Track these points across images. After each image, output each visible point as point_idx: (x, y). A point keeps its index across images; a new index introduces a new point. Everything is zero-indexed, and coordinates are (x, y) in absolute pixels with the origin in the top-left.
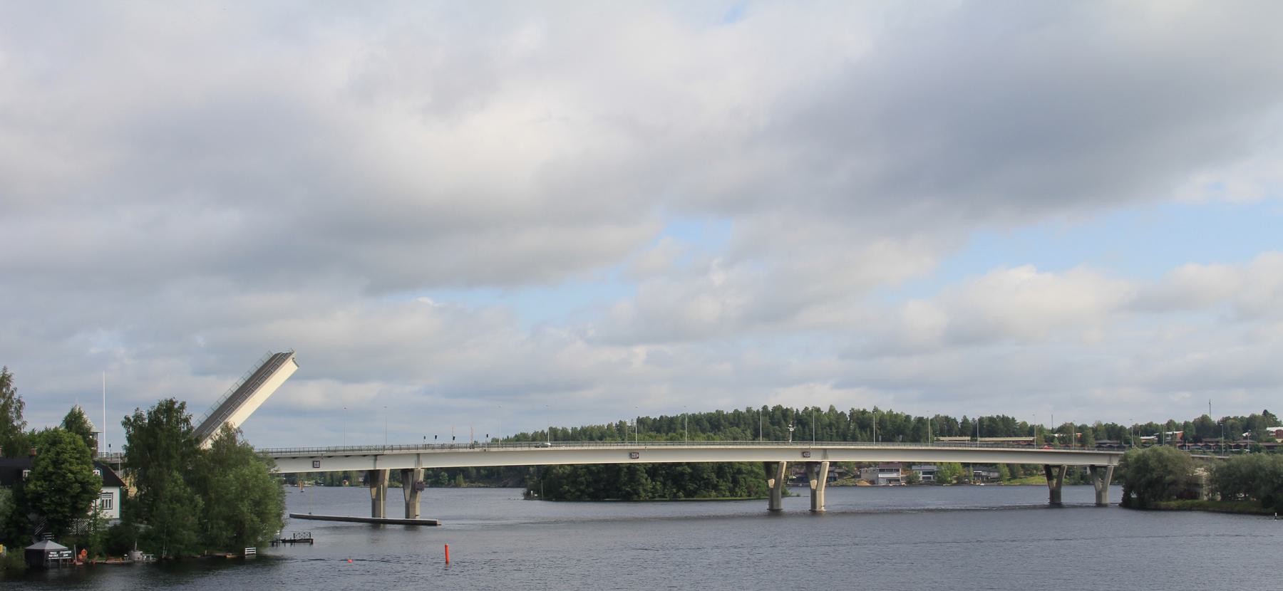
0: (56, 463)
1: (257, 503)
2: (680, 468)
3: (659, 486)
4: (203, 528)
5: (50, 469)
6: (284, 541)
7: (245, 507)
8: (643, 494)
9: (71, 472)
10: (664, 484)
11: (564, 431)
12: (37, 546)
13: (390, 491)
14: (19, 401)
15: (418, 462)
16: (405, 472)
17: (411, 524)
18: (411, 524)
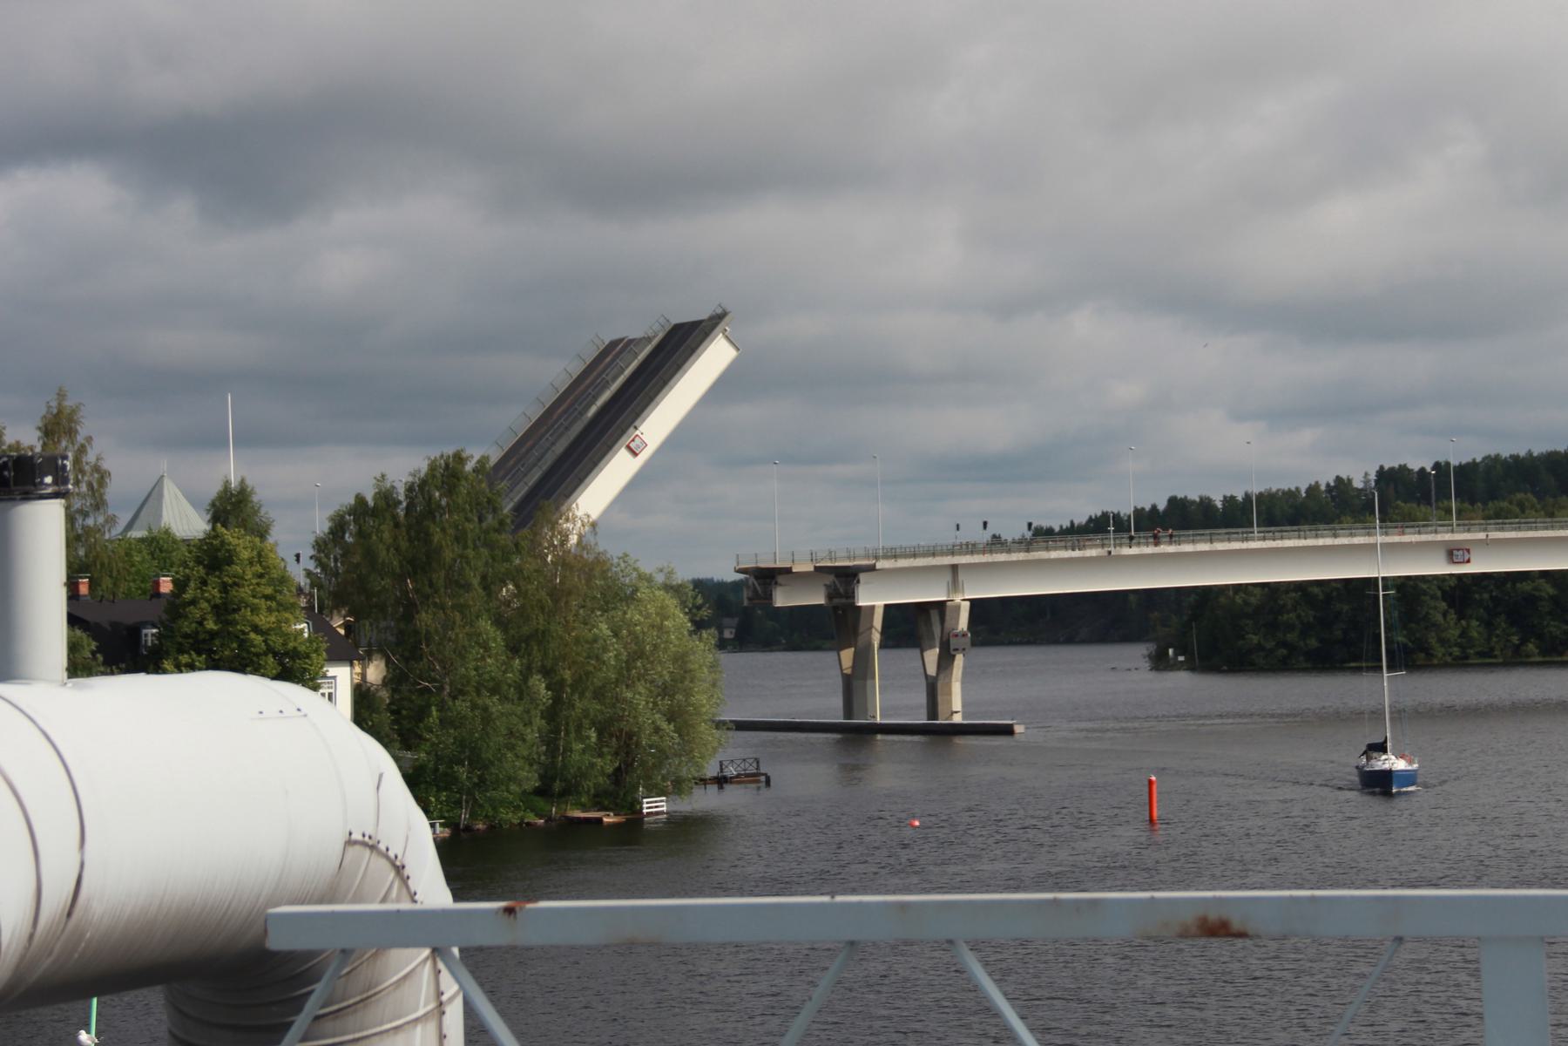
0: (224, 610)
1: (666, 691)
2: (1526, 587)
3: (1475, 630)
5: (211, 625)
6: (704, 782)
7: (639, 697)
8: (1439, 651)
10: (1489, 625)
11: (1206, 504)
14: (97, 469)
15: (955, 585)
16: (921, 609)
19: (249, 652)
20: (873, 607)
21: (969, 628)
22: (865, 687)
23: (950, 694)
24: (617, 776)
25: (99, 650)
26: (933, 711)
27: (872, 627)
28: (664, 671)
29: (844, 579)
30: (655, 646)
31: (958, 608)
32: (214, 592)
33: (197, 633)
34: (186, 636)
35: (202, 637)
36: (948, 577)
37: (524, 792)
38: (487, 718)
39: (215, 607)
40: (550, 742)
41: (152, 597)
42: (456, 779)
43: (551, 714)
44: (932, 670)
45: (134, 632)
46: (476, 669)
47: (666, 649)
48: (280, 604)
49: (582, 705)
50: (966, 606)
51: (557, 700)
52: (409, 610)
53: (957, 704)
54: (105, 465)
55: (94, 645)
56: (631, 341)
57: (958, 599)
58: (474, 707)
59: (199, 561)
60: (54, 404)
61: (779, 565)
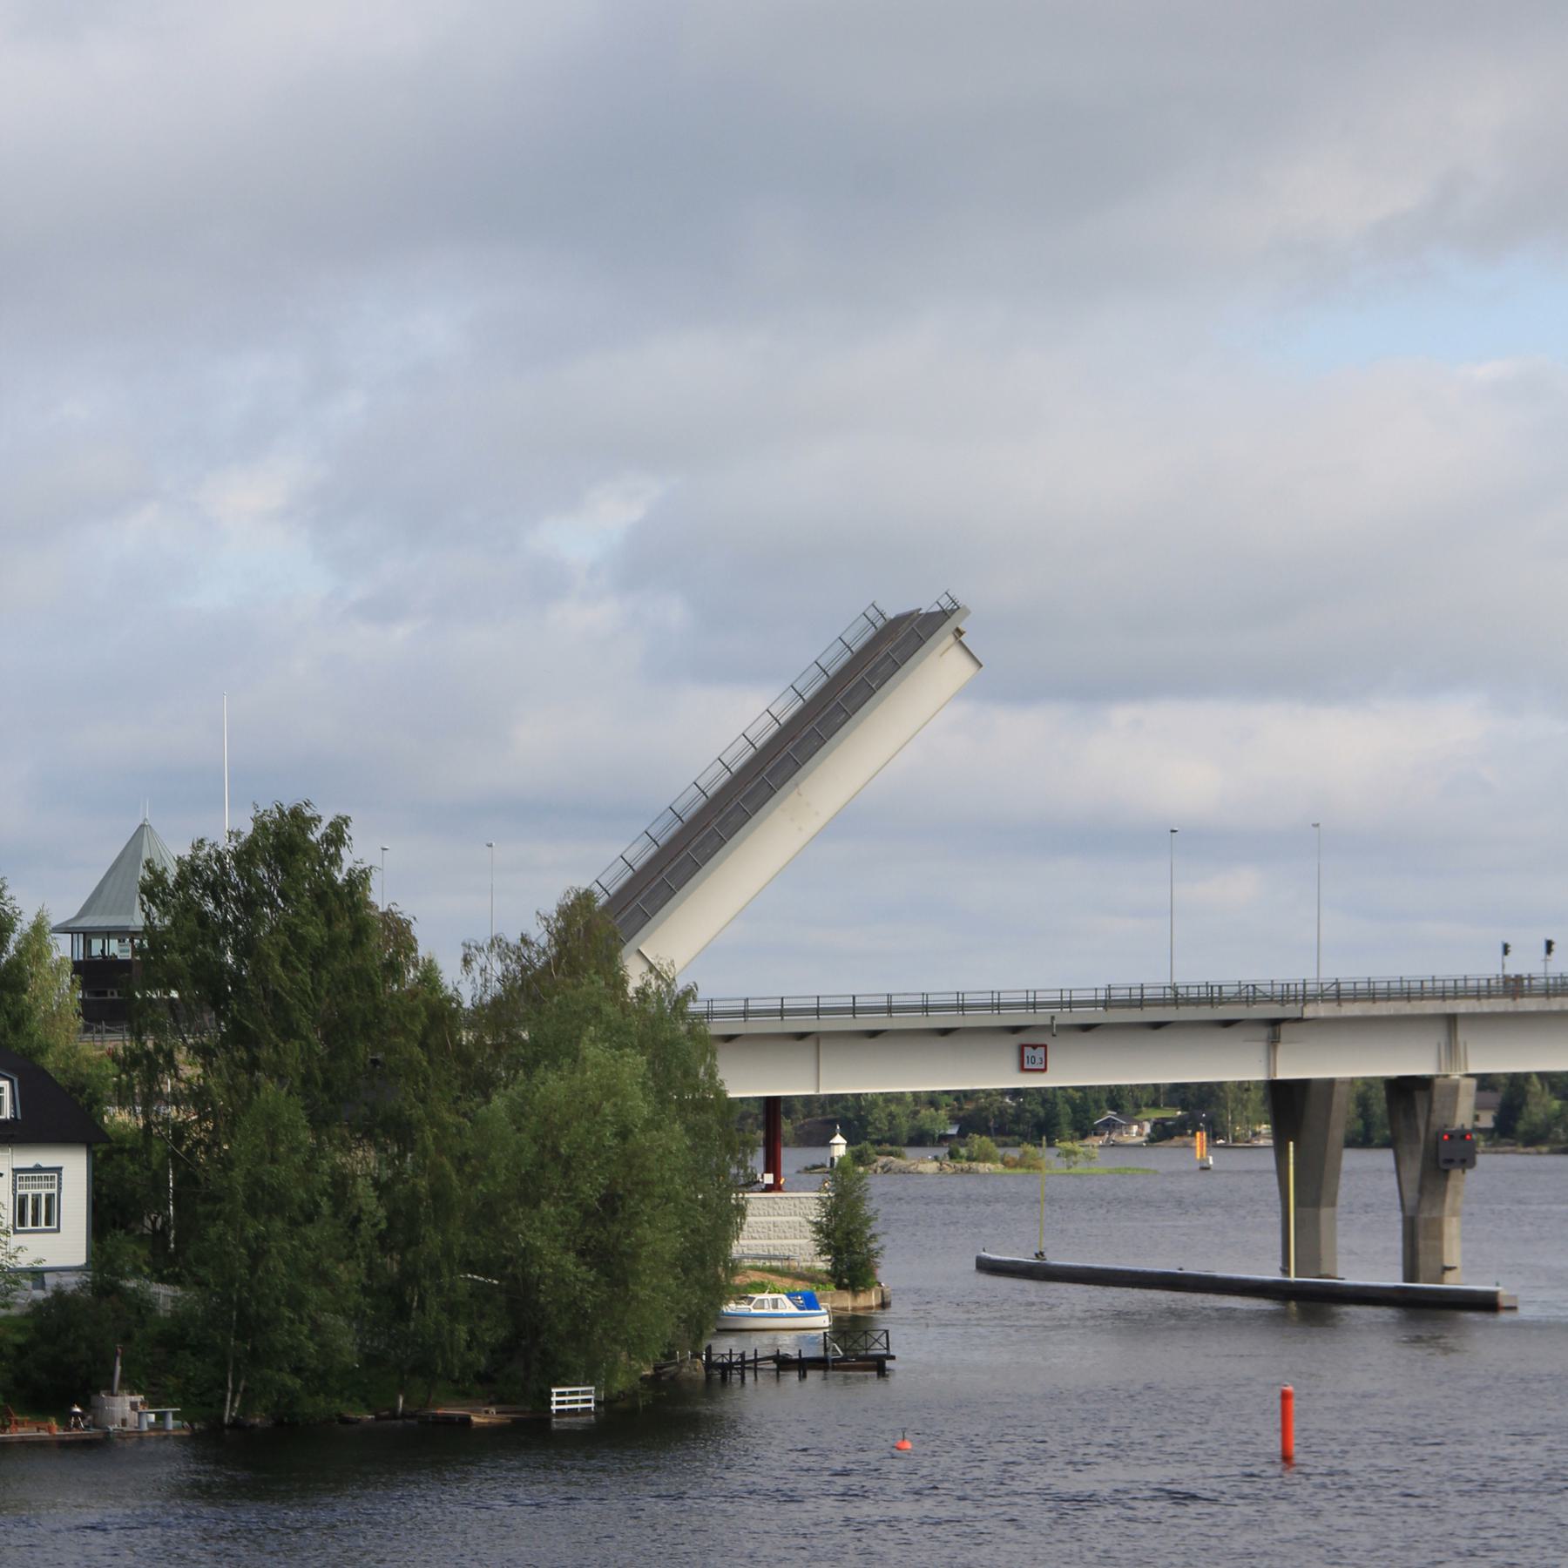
4: (392, 1301)
13: (1353, 1161)
15: (1452, 1049)
16: (1405, 1091)
17: (1428, 1308)
18: (1428, 1308)
31: (1455, 1088)
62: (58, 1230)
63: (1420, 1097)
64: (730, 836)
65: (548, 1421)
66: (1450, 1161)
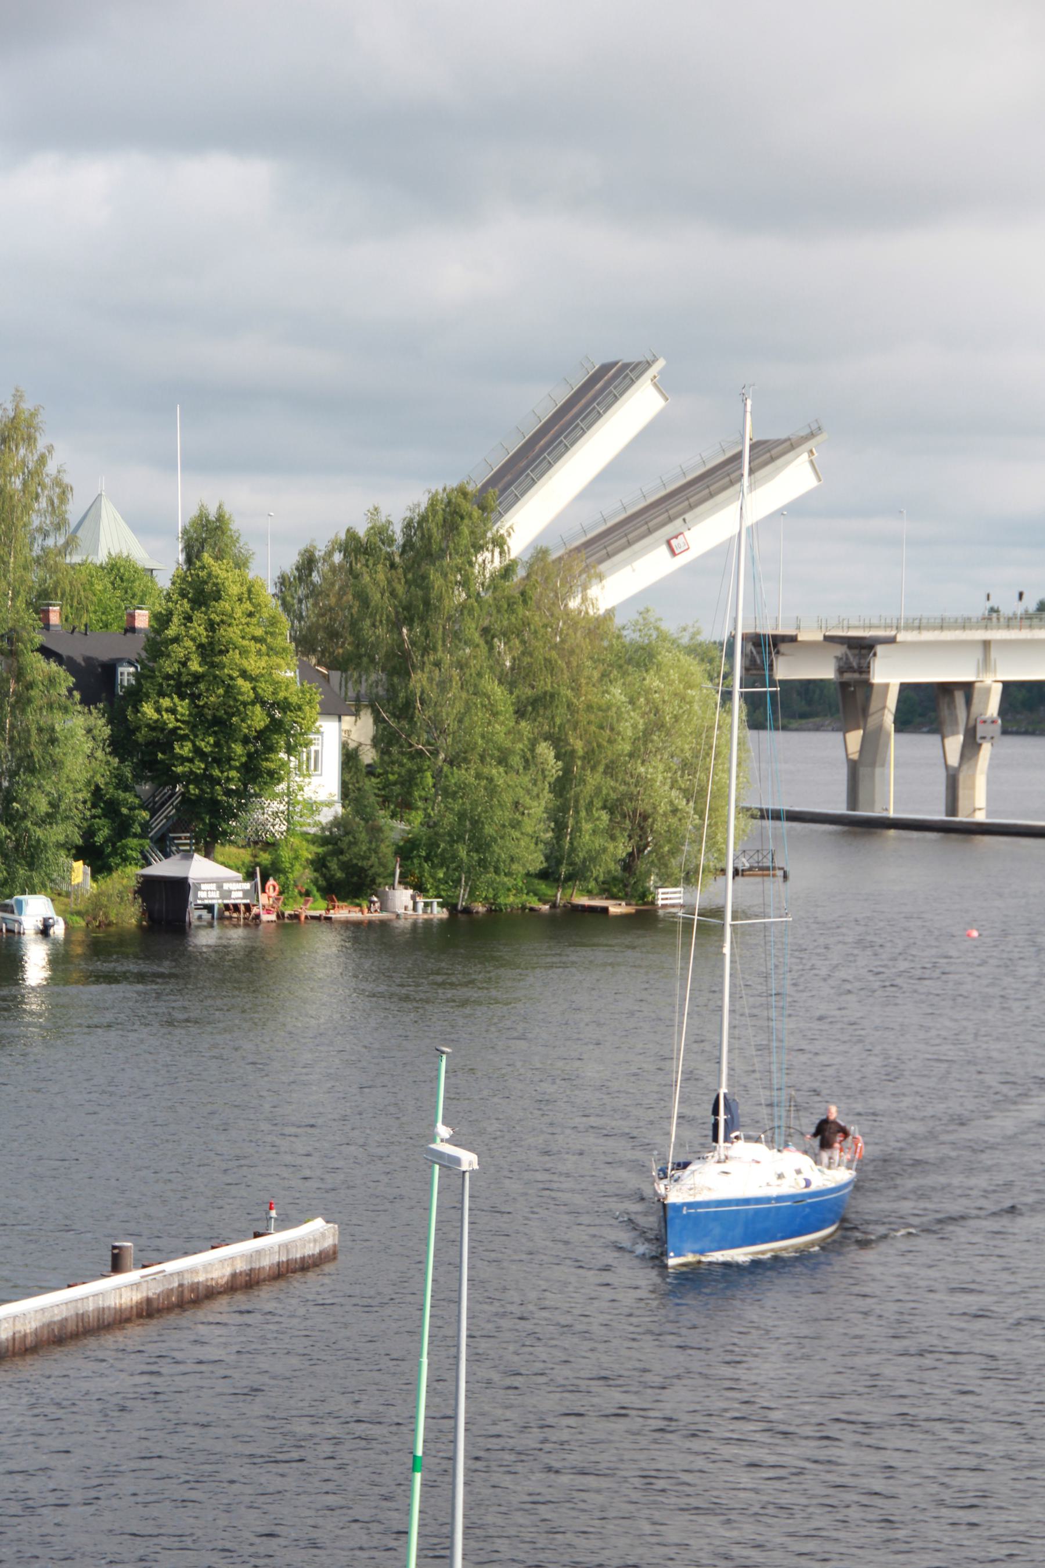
0: (210, 651)
5: (195, 666)
7: (655, 772)
9: (244, 674)
12: (163, 868)
14: (57, 482)
15: (986, 664)
16: (946, 689)
19: (236, 700)
20: (886, 686)
21: (1002, 712)
22: (872, 777)
23: (972, 787)
24: (628, 865)
25: (76, 687)
26: (952, 808)
27: (884, 708)
28: (686, 746)
29: (859, 650)
30: (676, 718)
31: (988, 690)
32: (198, 629)
33: (180, 674)
34: (168, 677)
35: (184, 679)
36: (979, 654)
37: (528, 874)
38: (492, 790)
39: (201, 646)
40: (558, 821)
41: (126, 631)
42: (454, 857)
43: (561, 786)
44: (953, 760)
45: (109, 669)
46: (483, 737)
47: (689, 722)
48: (270, 648)
49: (594, 779)
50: (997, 691)
51: (567, 770)
52: (400, 665)
53: (980, 799)
54: (67, 479)
55: (71, 680)
56: (626, 366)
57: (988, 679)
58: (478, 776)
59: (183, 595)
60: (10, 406)
61: (781, 631)
62: (321, 775)
63: (959, 697)
64: (523, 494)
65: (656, 911)
66: (983, 738)
